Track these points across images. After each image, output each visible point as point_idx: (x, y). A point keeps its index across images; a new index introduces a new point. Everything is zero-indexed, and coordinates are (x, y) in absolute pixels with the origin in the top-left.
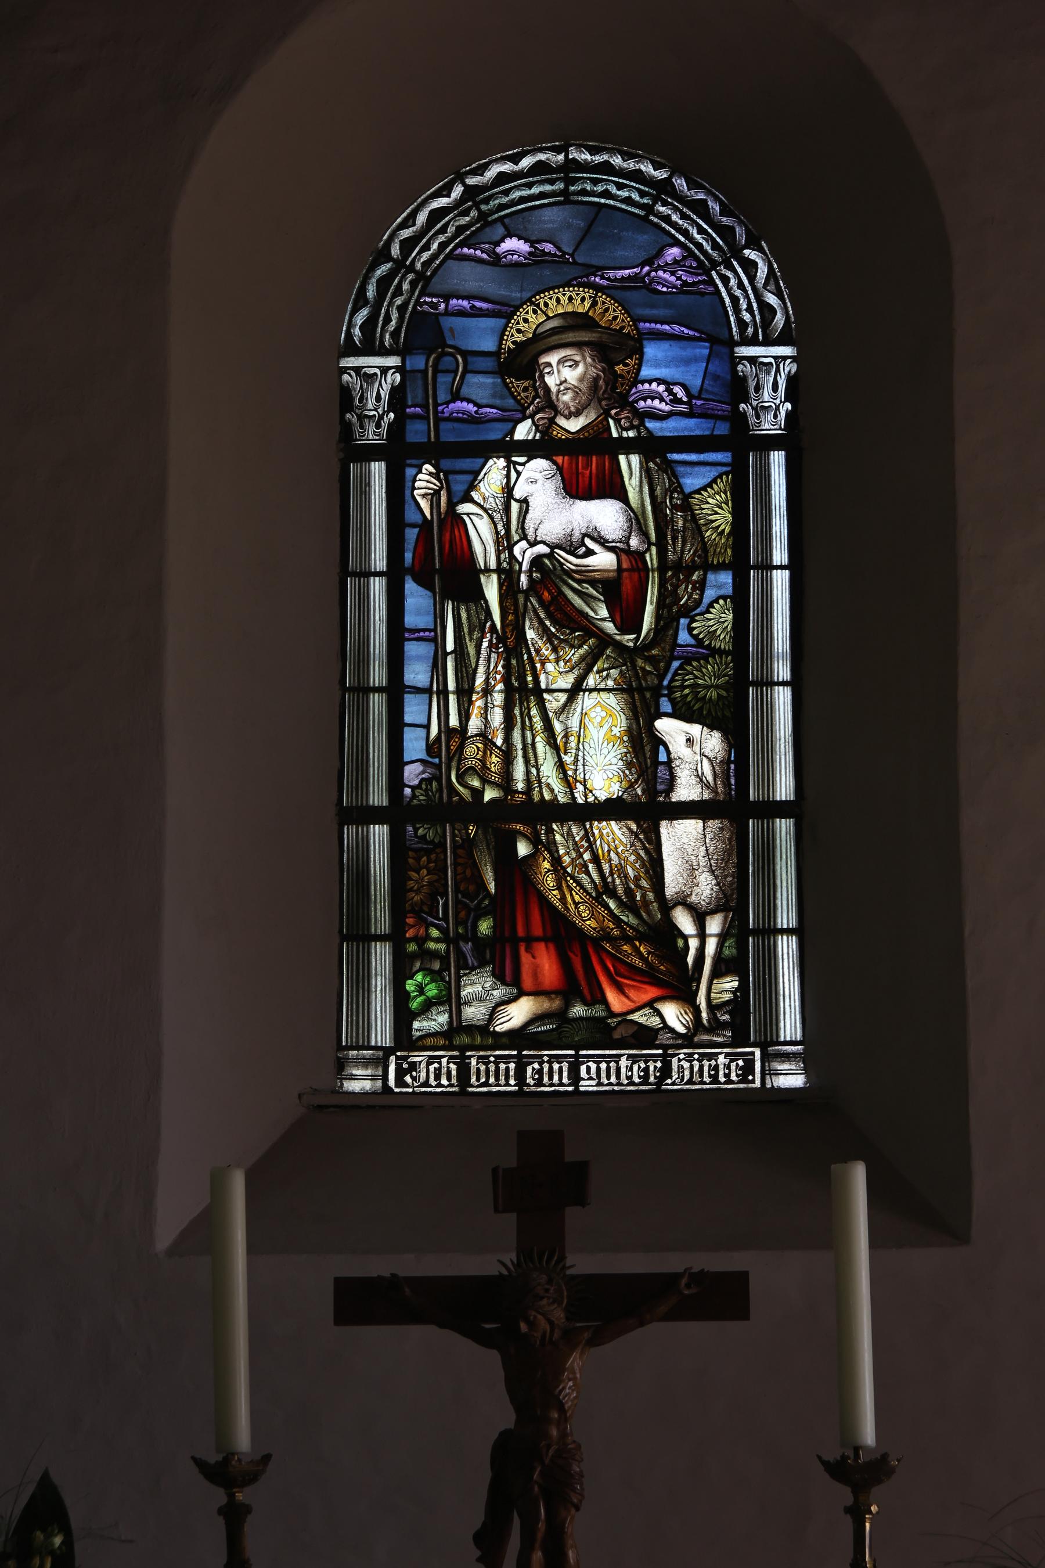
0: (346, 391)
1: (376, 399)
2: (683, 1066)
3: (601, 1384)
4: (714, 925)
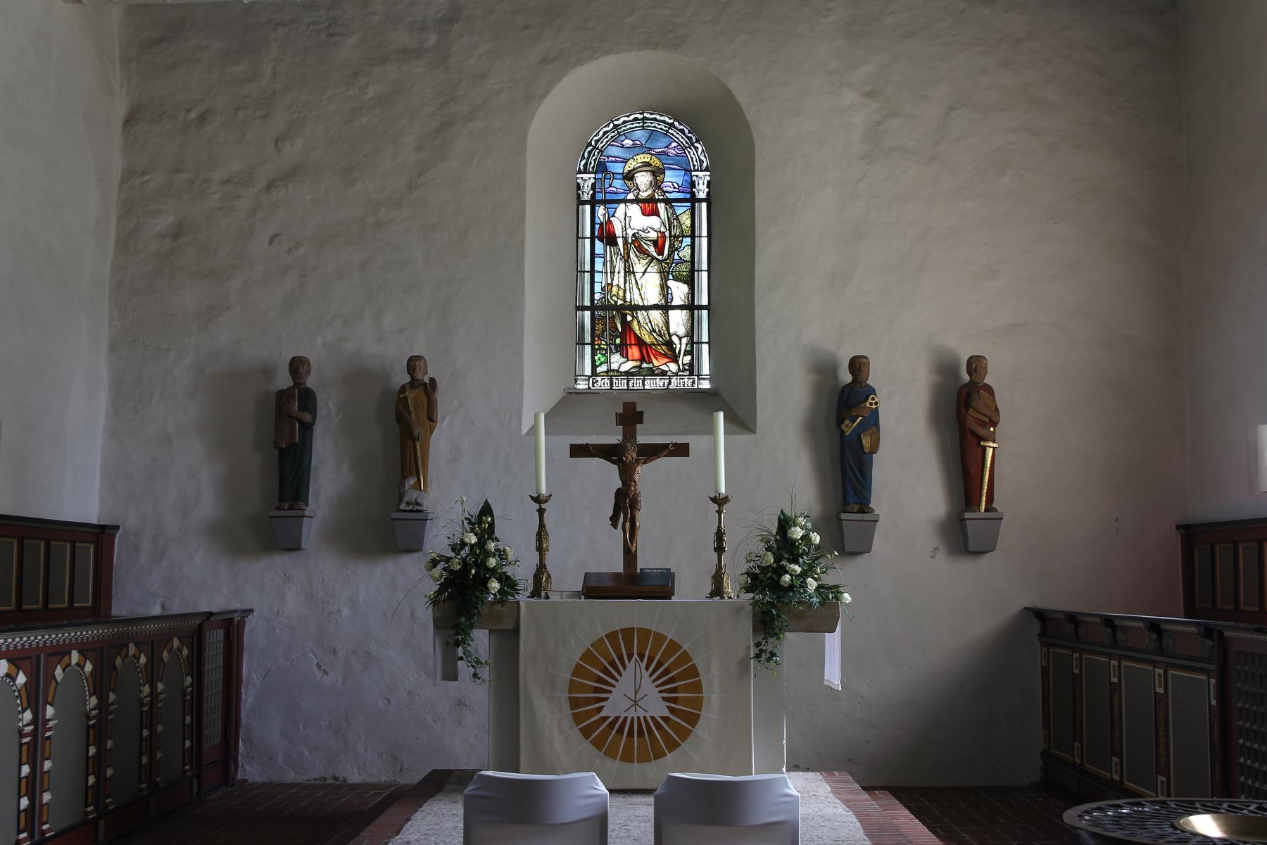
0: (578, 185)
1: (587, 187)
2: (675, 383)
3: (646, 474)
4: (685, 340)
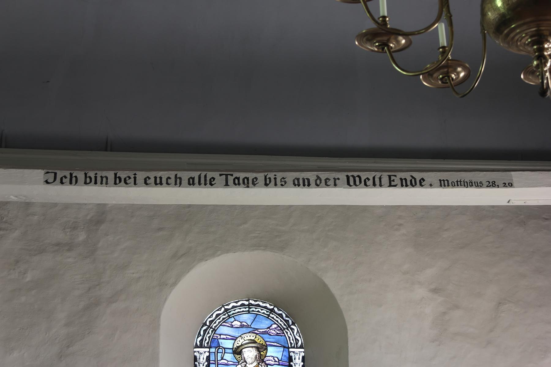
0: (195, 358)
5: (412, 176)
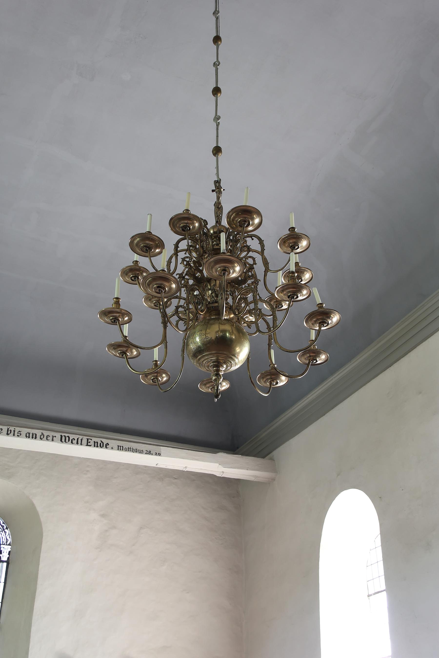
5: (101, 441)
